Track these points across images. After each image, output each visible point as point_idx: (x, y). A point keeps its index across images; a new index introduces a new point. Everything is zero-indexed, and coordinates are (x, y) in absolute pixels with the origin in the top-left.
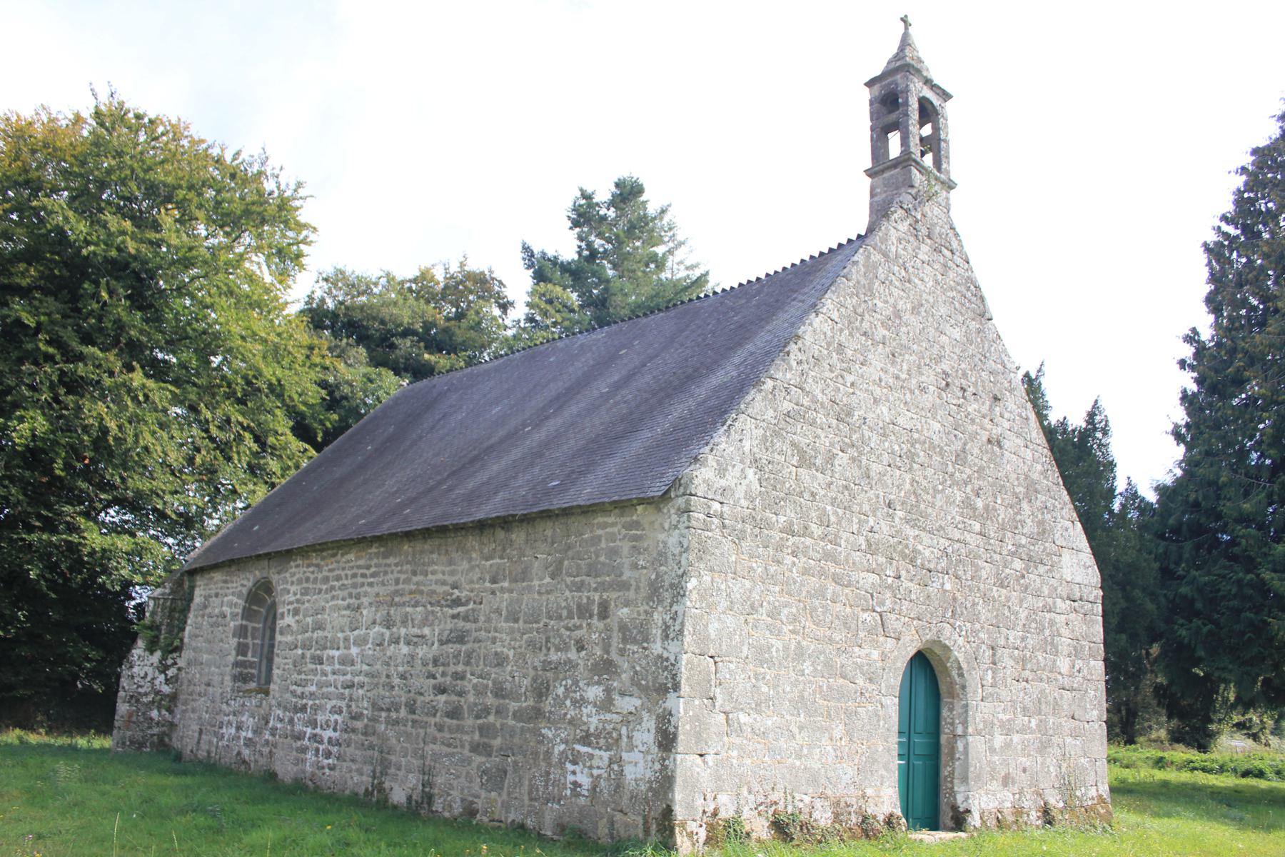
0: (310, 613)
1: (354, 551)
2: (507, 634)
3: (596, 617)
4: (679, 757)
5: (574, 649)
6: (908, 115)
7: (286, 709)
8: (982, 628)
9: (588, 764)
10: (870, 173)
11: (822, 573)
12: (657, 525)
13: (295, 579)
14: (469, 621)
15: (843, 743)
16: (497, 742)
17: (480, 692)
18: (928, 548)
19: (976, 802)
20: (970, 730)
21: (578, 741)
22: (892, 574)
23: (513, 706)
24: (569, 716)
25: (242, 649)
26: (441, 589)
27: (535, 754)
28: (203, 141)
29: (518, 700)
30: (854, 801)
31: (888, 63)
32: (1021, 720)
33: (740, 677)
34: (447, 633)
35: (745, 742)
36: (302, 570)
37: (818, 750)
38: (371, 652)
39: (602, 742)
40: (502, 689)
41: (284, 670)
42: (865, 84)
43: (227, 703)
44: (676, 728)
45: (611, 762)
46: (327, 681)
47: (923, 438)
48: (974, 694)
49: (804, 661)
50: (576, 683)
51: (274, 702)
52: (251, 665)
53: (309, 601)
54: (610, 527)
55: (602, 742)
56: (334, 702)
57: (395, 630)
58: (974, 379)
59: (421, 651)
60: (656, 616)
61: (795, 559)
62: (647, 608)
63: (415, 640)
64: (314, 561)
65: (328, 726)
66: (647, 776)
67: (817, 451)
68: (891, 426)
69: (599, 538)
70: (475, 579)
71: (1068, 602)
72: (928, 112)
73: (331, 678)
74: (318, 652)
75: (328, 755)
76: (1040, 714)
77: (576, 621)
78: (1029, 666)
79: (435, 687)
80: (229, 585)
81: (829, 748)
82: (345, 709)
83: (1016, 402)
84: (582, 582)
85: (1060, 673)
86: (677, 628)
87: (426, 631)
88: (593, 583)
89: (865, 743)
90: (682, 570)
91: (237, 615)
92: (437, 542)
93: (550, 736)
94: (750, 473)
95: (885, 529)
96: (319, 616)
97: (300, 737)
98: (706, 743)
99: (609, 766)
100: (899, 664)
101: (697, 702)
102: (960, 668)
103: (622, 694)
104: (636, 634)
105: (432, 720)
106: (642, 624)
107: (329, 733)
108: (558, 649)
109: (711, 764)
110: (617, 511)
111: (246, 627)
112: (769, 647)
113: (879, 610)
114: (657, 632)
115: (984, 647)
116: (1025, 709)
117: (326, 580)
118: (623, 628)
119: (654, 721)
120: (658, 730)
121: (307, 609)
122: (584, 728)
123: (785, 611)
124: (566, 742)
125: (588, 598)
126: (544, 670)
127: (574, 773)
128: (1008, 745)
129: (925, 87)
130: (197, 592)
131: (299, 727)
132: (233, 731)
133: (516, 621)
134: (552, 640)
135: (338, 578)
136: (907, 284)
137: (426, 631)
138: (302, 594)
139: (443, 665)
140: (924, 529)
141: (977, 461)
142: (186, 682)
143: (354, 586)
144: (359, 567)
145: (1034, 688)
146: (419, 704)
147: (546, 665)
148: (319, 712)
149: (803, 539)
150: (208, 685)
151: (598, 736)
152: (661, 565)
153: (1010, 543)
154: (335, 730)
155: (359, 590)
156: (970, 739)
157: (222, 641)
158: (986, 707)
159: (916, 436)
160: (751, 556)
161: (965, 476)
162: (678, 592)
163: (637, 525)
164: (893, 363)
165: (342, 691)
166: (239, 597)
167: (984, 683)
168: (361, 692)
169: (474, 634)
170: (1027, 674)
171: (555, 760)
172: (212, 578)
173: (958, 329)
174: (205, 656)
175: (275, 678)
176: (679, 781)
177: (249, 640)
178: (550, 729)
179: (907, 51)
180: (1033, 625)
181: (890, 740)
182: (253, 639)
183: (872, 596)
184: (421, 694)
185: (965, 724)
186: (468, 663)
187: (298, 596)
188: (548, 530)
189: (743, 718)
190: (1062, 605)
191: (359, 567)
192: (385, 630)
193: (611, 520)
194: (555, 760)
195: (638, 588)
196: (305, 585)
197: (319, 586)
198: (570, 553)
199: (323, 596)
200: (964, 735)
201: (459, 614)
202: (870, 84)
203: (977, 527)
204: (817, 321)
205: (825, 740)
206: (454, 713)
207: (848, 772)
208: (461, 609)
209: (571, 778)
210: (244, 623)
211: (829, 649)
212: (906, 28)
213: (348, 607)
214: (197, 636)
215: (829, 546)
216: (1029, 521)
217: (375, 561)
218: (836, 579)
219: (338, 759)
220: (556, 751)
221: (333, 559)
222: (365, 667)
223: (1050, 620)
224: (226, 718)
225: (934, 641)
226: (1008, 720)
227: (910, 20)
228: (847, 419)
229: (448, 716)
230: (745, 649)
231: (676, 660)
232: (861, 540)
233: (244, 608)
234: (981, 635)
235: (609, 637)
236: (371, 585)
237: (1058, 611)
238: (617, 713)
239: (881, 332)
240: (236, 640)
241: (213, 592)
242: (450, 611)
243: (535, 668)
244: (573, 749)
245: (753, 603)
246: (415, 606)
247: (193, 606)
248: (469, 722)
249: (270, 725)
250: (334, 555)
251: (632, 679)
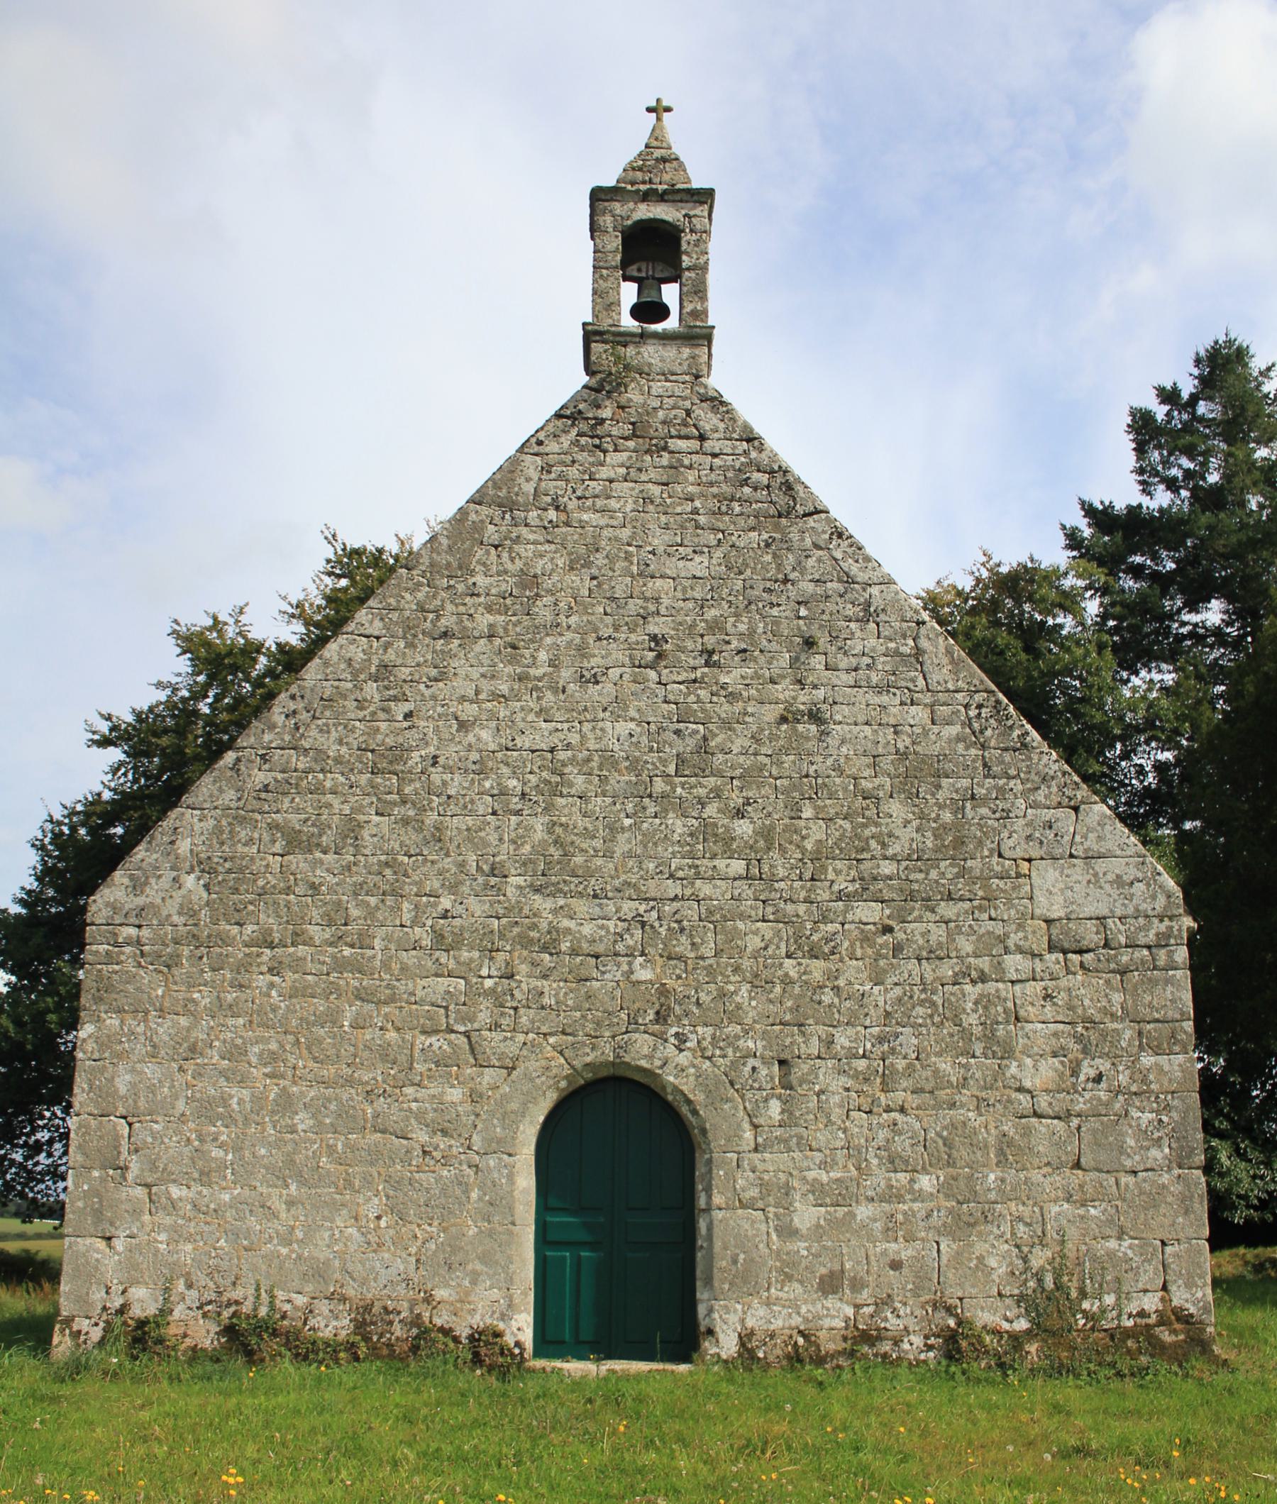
19: (733, 1319)
22: (494, 973)
98: (112, 1224)
109: (120, 1248)
189: (175, 1191)
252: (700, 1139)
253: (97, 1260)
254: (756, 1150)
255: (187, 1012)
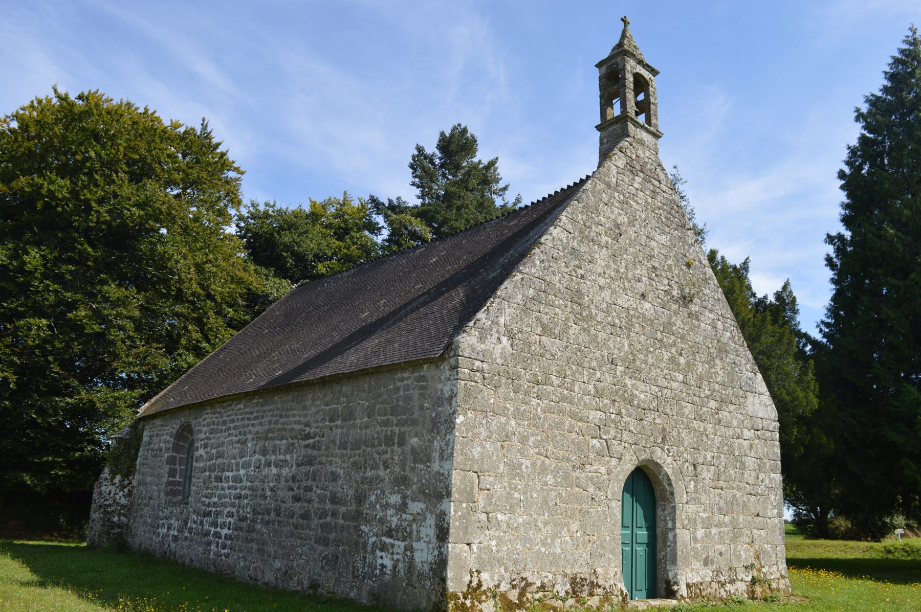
0: (215, 446)
1: (243, 402)
2: (340, 458)
3: (396, 445)
4: (450, 545)
5: (382, 468)
6: (625, 86)
7: (198, 514)
8: (686, 450)
9: (391, 551)
10: (599, 128)
11: (561, 411)
12: (436, 378)
13: (205, 423)
14: (316, 449)
15: (579, 535)
16: (332, 536)
17: (322, 500)
18: (643, 393)
19: (683, 578)
20: (678, 525)
21: (385, 535)
22: (614, 412)
23: (343, 509)
24: (378, 517)
25: (172, 473)
26: (297, 427)
27: (357, 543)
28: (32, 102)
29: (346, 505)
30: (587, 577)
31: (613, 50)
32: (718, 517)
33: (498, 487)
34: (301, 458)
35: (502, 534)
36: (210, 416)
37: (559, 540)
38: (252, 473)
39: (400, 534)
40: (335, 497)
41: (198, 487)
42: (596, 66)
43: (162, 511)
44: (449, 524)
45: (406, 549)
46: (224, 494)
47: (637, 314)
48: (681, 497)
49: (547, 475)
50: (383, 492)
51: (191, 510)
52: (179, 484)
53: (214, 438)
54: (408, 378)
55: (400, 534)
56: (228, 509)
57: (268, 457)
58: (677, 272)
59: (285, 471)
60: (435, 443)
61: (539, 401)
62: (430, 437)
63: (281, 463)
64: (218, 410)
65: (225, 526)
66: (429, 560)
67: (556, 325)
68: (613, 306)
69: (399, 388)
70: (319, 419)
71: (752, 431)
72: (641, 84)
73: (227, 492)
74: (219, 473)
75: (224, 547)
76: (732, 512)
77: (383, 448)
78: (723, 478)
79: (293, 497)
80: (165, 428)
81: (568, 538)
82: (235, 514)
83: (713, 292)
84: (388, 420)
85: (747, 483)
86: (449, 451)
87: (288, 457)
88: (394, 419)
89: (596, 534)
90: (453, 410)
91: (169, 449)
92: (296, 393)
93: (366, 531)
94: (504, 340)
95: (609, 379)
96: (220, 448)
97: (207, 534)
98: (472, 535)
99: (404, 552)
100: (621, 477)
101: (464, 505)
102: (669, 480)
103: (413, 500)
104: (422, 456)
105: (291, 521)
106: (426, 449)
107: (225, 531)
108: (372, 468)
109: (475, 550)
110: (411, 369)
111: (175, 457)
112: (520, 465)
113: (605, 438)
114: (436, 455)
115: (687, 464)
116: (720, 509)
117: (225, 423)
118: (414, 451)
119: (434, 519)
120: (436, 525)
121: (213, 443)
122: (389, 525)
123: (532, 439)
124: (377, 535)
125: (392, 431)
126: (363, 483)
127: (382, 557)
128: (708, 535)
129: (638, 66)
130: (145, 434)
131: (206, 527)
132: (165, 530)
133: (345, 449)
134: (368, 462)
135: (233, 421)
136: (625, 206)
137: (288, 457)
138: (210, 433)
139: (298, 481)
140: (640, 380)
141: (680, 330)
142: (137, 497)
143: (243, 426)
144: (246, 413)
145: (728, 494)
146: (282, 509)
147: (364, 481)
148: (219, 516)
149: (545, 387)
150: (150, 498)
151: (397, 531)
152: (439, 407)
153: (706, 388)
154: (229, 529)
155: (245, 429)
156: (678, 531)
157: (159, 467)
158: (691, 508)
159: (632, 312)
160: (506, 400)
161: (671, 341)
162: (450, 425)
163: (422, 378)
164: (615, 262)
165: (234, 501)
166: (170, 437)
167: (688, 490)
168: (246, 501)
169: (319, 459)
170: (721, 483)
171: (369, 549)
172: (154, 424)
173: (664, 237)
174: (149, 478)
175: (192, 492)
176: (451, 563)
177: (177, 466)
178: (366, 525)
179: (626, 42)
180: (726, 448)
181: (615, 532)
182: (180, 465)
183: (599, 427)
184: (284, 502)
185: (674, 520)
186: (314, 480)
187: (207, 435)
188: (365, 384)
189: (500, 517)
190: (747, 434)
191: (246, 413)
192: (261, 457)
193: (406, 375)
194: (369, 549)
195: (424, 423)
196: (212, 427)
197: (220, 427)
198: (380, 400)
199: (223, 434)
200: (674, 528)
201: (309, 444)
202: (599, 65)
203: (681, 378)
204: (555, 231)
205: (565, 531)
206: (305, 516)
207: (583, 554)
208: (311, 441)
209: (379, 561)
210: (174, 454)
211: (568, 466)
212: (625, 26)
213: (238, 442)
214: (144, 464)
215: (566, 392)
216: (721, 373)
217: (256, 408)
218: (572, 416)
219: (231, 549)
220: (370, 542)
221: (230, 408)
222: (249, 484)
223: (739, 444)
224: (161, 522)
225: (649, 460)
226: (708, 518)
227: (628, 20)
228: (579, 301)
229: (301, 518)
230: (501, 466)
231: (448, 475)
232: (591, 387)
233: (174, 443)
234: (685, 455)
235: (405, 459)
236: (253, 425)
237: (745, 437)
238: (410, 514)
239: (604, 239)
240: (168, 466)
241: (155, 433)
242: (304, 443)
243: (357, 482)
244: (381, 540)
245: (507, 433)
246: (281, 439)
247: (143, 444)
248: (315, 522)
249: (189, 526)
250: (231, 405)
251: (419, 488)
252: (669, 497)
253: (465, 557)
254: (687, 503)
255: (505, 415)
